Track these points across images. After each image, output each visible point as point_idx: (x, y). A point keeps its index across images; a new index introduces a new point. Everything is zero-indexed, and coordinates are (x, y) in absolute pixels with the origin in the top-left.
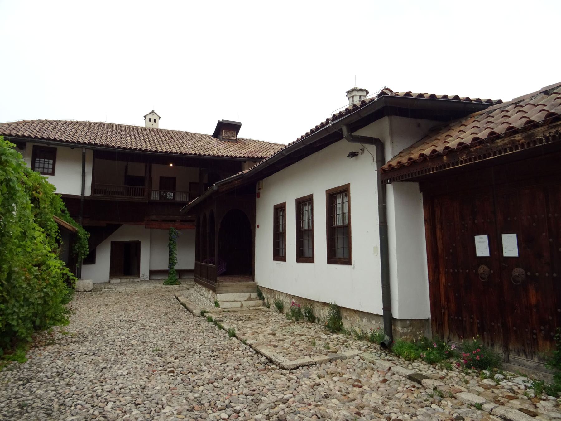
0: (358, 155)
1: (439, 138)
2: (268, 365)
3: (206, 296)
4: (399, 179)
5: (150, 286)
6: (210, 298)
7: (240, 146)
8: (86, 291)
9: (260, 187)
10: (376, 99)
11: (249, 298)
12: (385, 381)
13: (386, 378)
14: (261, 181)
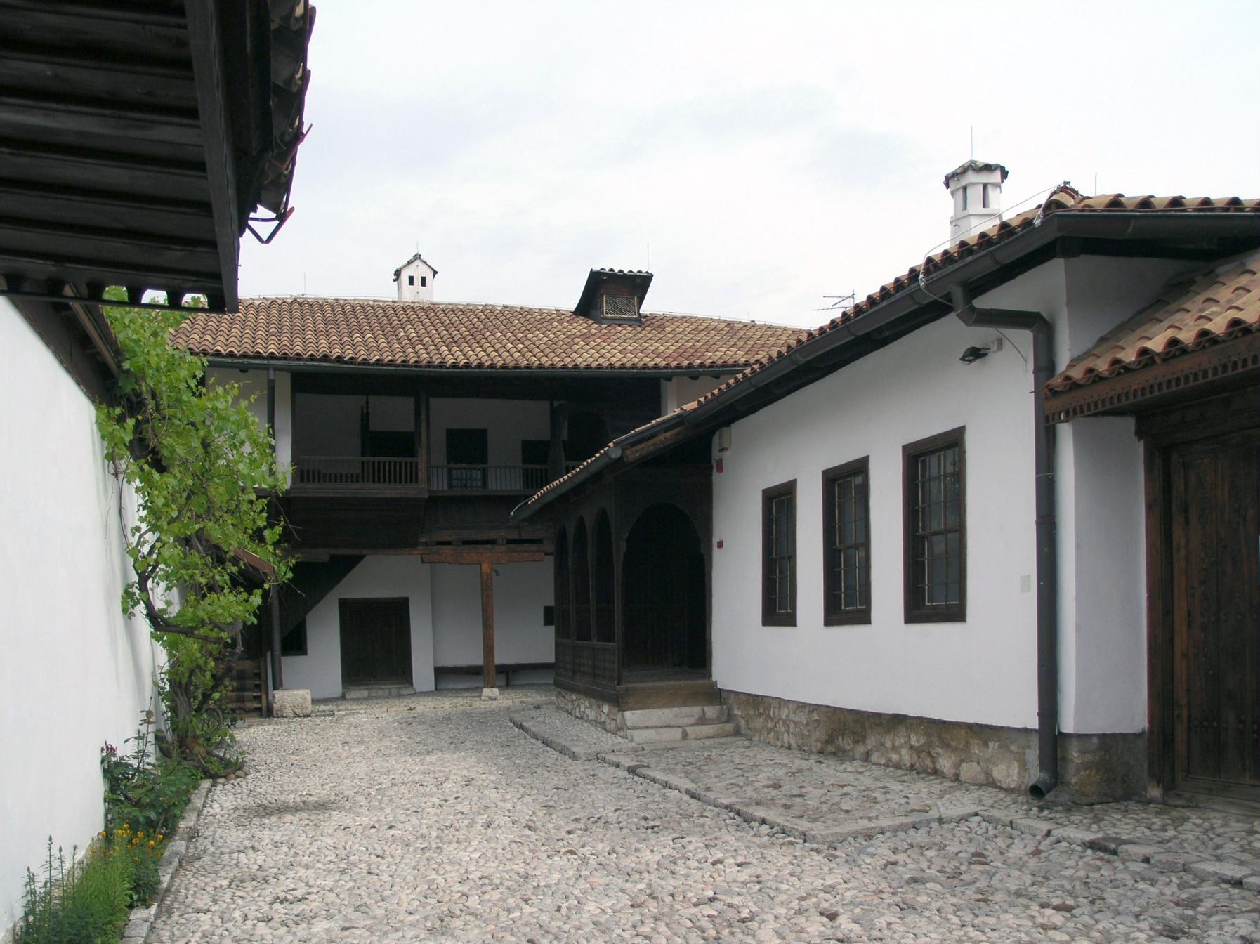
0: (986, 355)
1: (1187, 306)
2: (777, 838)
3: (590, 718)
4: (1089, 409)
5: (445, 704)
6: (604, 722)
7: (650, 335)
8: (299, 716)
9: (725, 446)
10: (1037, 222)
11: (700, 718)
12: (1037, 853)
13: (1040, 848)
14: (725, 430)
